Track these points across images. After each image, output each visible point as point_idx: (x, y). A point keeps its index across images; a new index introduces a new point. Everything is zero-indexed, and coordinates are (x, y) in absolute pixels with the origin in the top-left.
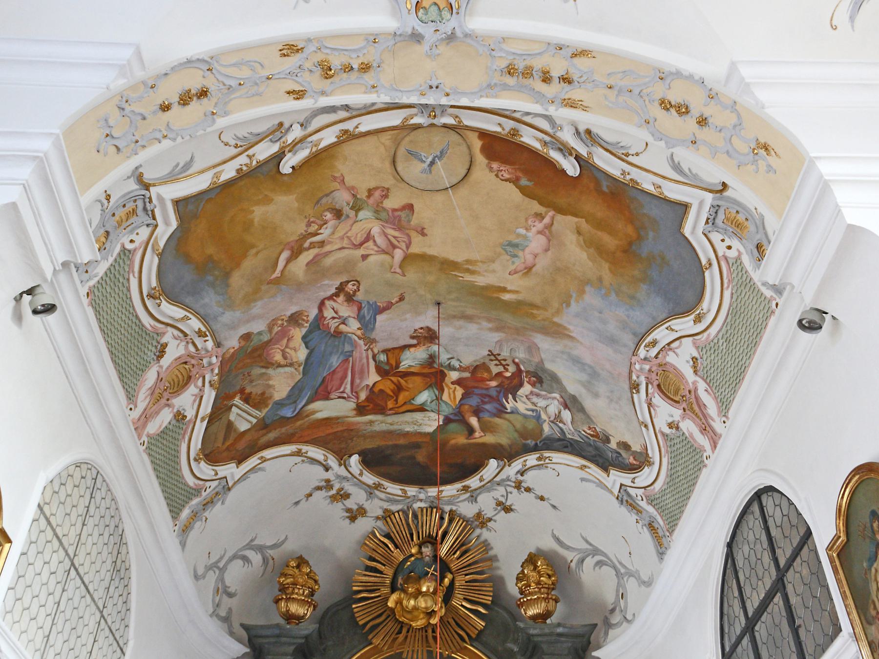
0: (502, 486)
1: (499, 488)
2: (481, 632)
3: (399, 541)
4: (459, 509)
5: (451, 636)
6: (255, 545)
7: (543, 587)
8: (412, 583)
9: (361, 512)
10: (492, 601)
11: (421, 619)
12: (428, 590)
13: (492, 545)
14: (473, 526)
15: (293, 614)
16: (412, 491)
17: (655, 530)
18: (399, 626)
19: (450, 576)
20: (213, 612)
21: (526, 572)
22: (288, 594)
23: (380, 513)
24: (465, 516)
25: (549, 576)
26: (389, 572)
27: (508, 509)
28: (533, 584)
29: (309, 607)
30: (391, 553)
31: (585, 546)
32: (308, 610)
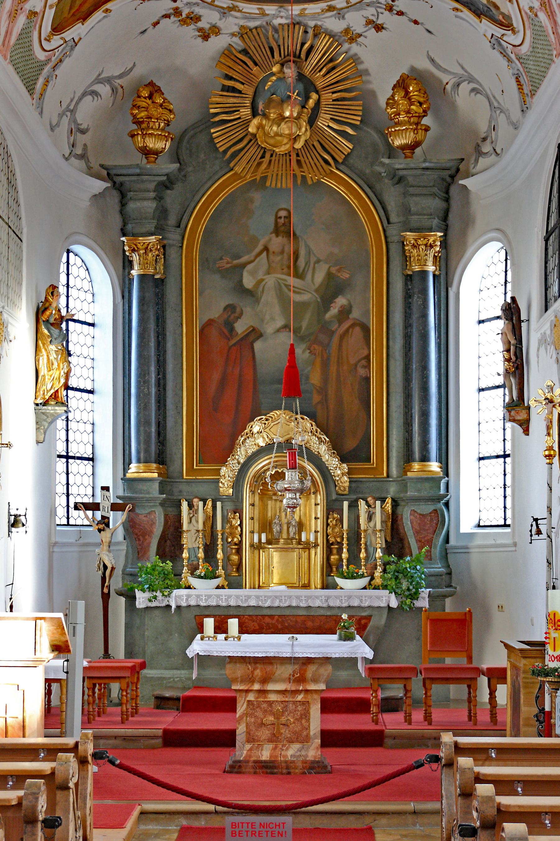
0: (373, 7)
1: (369, 8)
2: (348, 156)
3: (258, 58)
4: (325, 24)
5: (315, 159)
6: (102, 78)
7: (413, 116)
8: (274, 108)
9: (215, 30)
10: (361, 121)
11: (285, 144)
12: (291, 114)
13: (363, 59)
14: (340, 41)
15: (151, 149)
16: (271, 9)
17: (521, 85)
18: (262, 151)
19: (314, 96)
20: (70, 153)
21: (396, 98)
22: (144, 129)
23: (236, 29)
24: (331, 31)
25: (421, 104)
26: (249, 91)
27: (379, 28)
28: (402, 113)
29: (167, 141)
30: (250, 71)
31: (461, 72)
32: (166, 145)
